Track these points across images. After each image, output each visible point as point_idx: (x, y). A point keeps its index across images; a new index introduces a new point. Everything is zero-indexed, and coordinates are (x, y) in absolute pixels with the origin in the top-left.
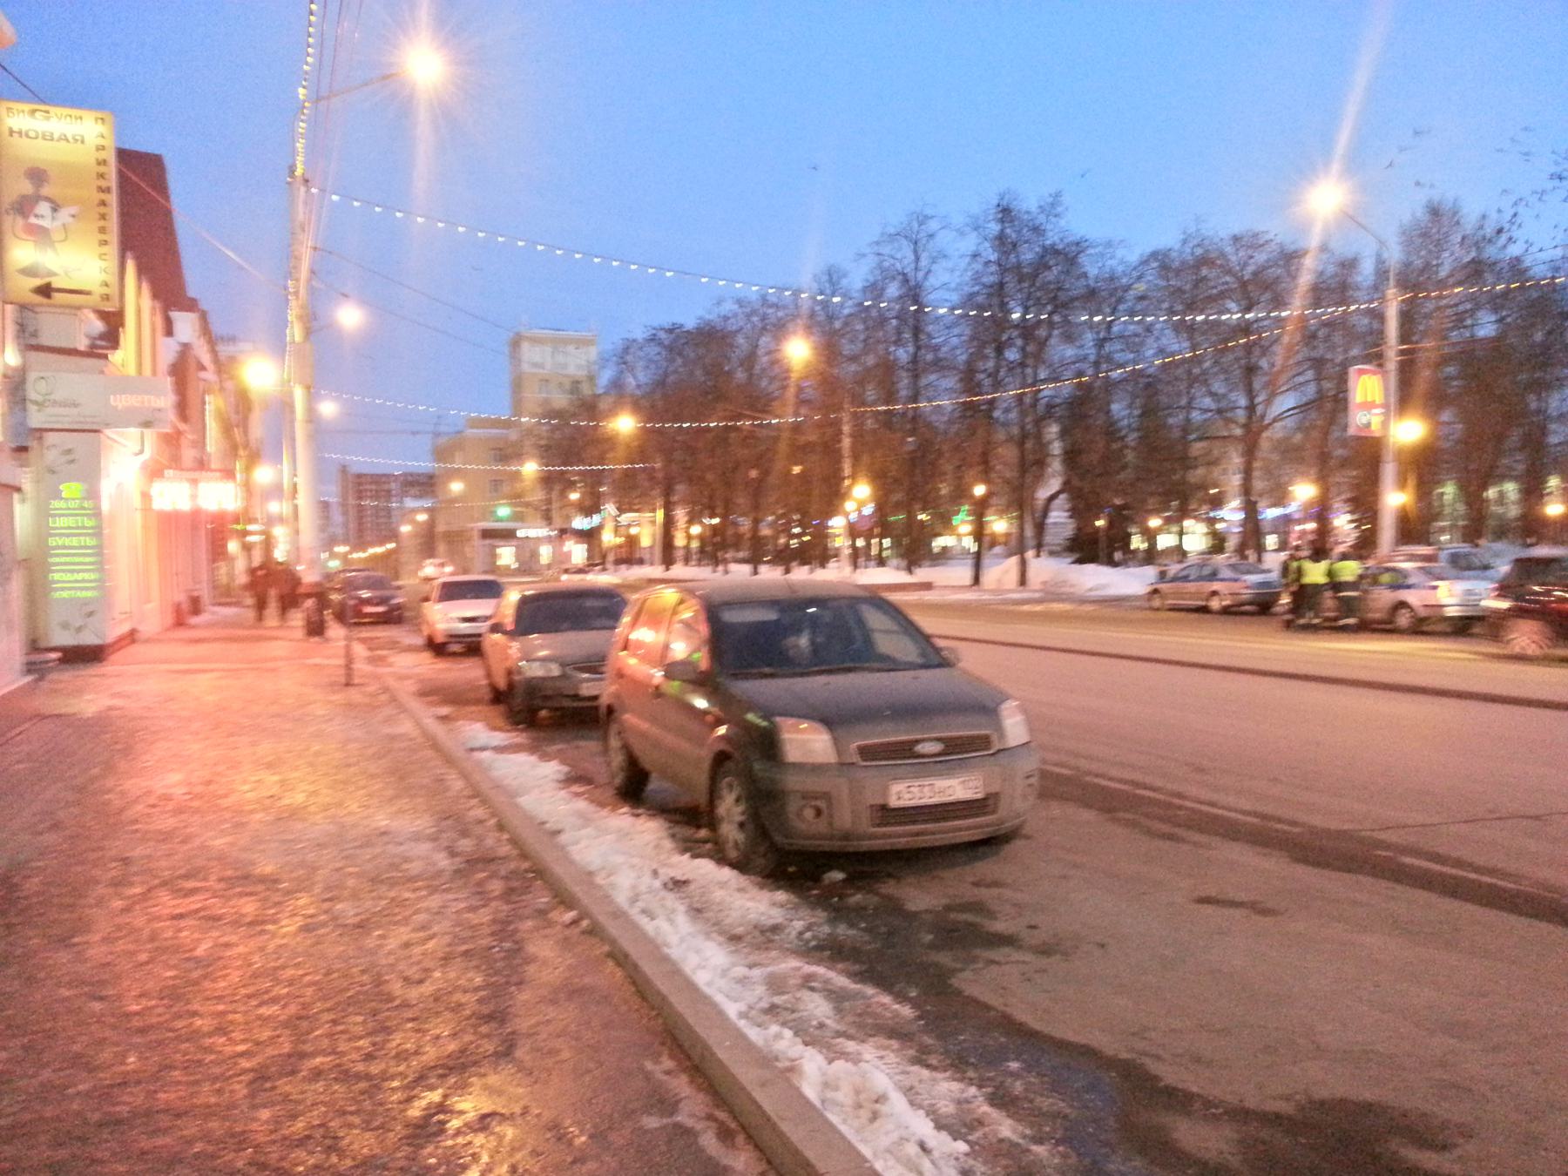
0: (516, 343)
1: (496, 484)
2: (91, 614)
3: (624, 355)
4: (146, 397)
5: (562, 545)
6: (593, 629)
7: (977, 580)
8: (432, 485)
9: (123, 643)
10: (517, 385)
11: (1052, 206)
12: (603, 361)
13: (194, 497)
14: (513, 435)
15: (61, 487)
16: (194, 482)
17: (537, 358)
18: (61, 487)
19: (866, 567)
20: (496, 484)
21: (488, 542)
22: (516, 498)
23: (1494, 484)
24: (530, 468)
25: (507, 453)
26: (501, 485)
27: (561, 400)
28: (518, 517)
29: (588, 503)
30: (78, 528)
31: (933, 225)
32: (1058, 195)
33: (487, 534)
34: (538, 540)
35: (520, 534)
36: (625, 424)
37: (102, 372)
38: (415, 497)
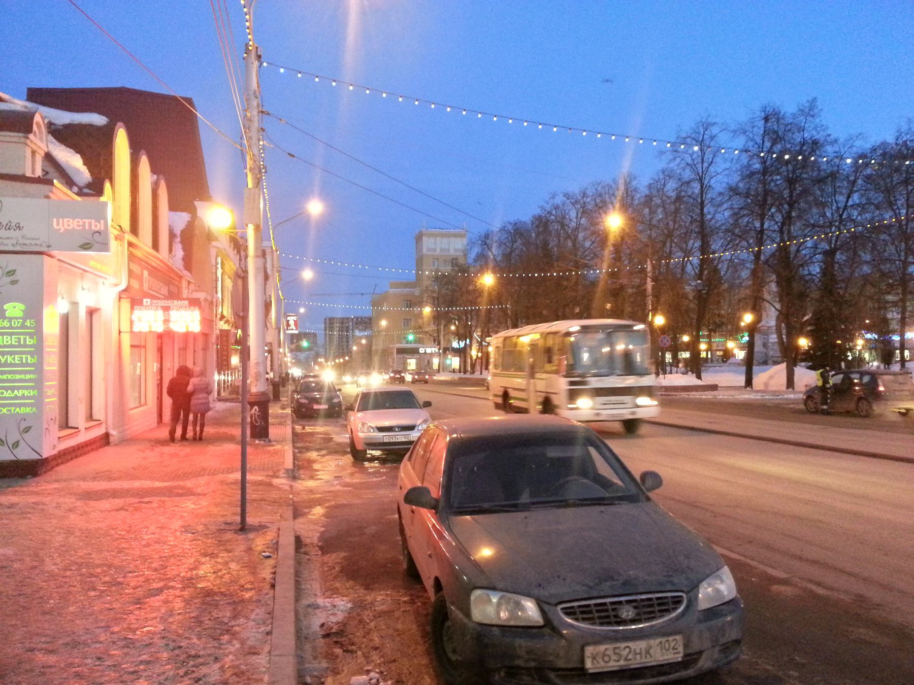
0: (419, 238)
1: (407, 322)
2: (27, 430)
3: (485, 241)
4: (87, 221)
5: (445, 358)
6: (564, 504)
7: (749, 382)
8: (370, 323)
9: (86, 449)
10: (420, 263)
11: (810, 110)
12: (472, 243)
13: (166, 321)
14: (417, 292)
15: (5, 307)
16: (166, 309)
17: (432, 246)
18: (5, 307)
19: (671, 373)
20: (407, 322)
21: (401, 356)
22: (419, 329)
23: (722, 336)
24: (427, 310)
25: (413, 302)
26: (409, 321)
27: (447, 269)
28: (419, 341)
29: (462, 331)
30: (20, 346)
31: (715, 130)
32: (814, 100)
33: (401, 351)
34: (432, 354)
35: (422, 350)
36: (488, 280)
37: (47, 197)
38: (360, 330)
